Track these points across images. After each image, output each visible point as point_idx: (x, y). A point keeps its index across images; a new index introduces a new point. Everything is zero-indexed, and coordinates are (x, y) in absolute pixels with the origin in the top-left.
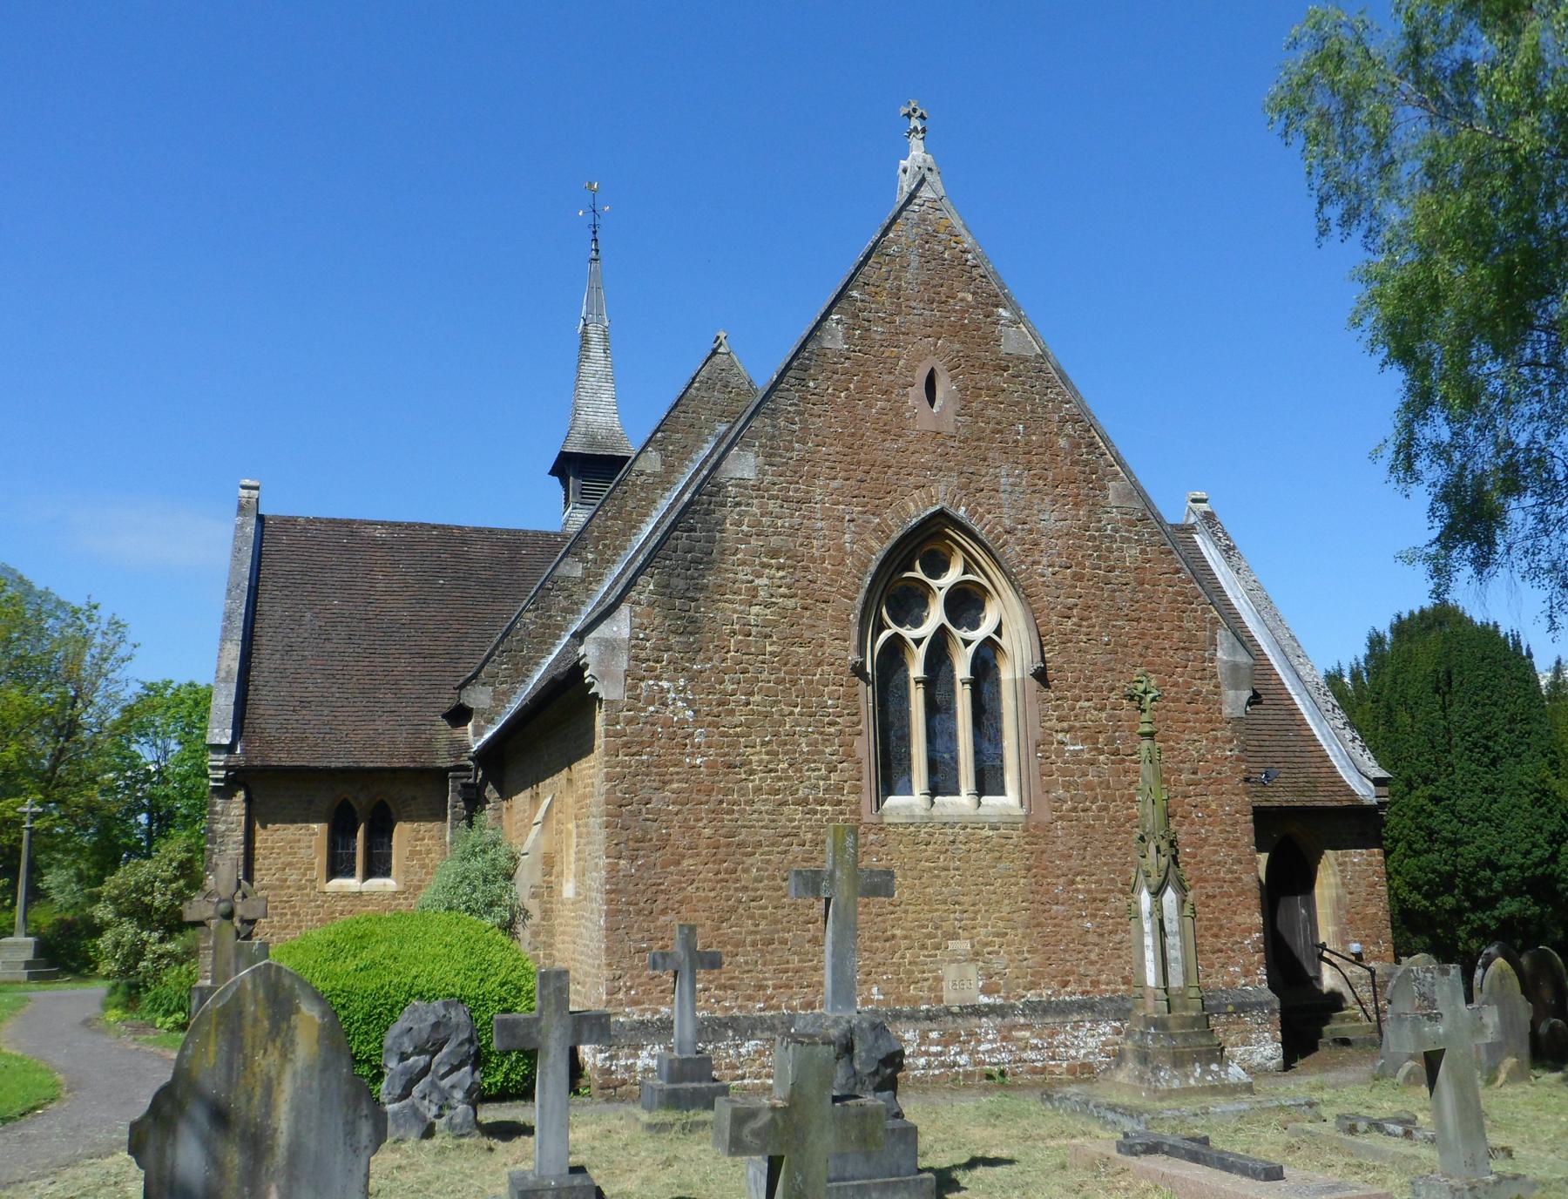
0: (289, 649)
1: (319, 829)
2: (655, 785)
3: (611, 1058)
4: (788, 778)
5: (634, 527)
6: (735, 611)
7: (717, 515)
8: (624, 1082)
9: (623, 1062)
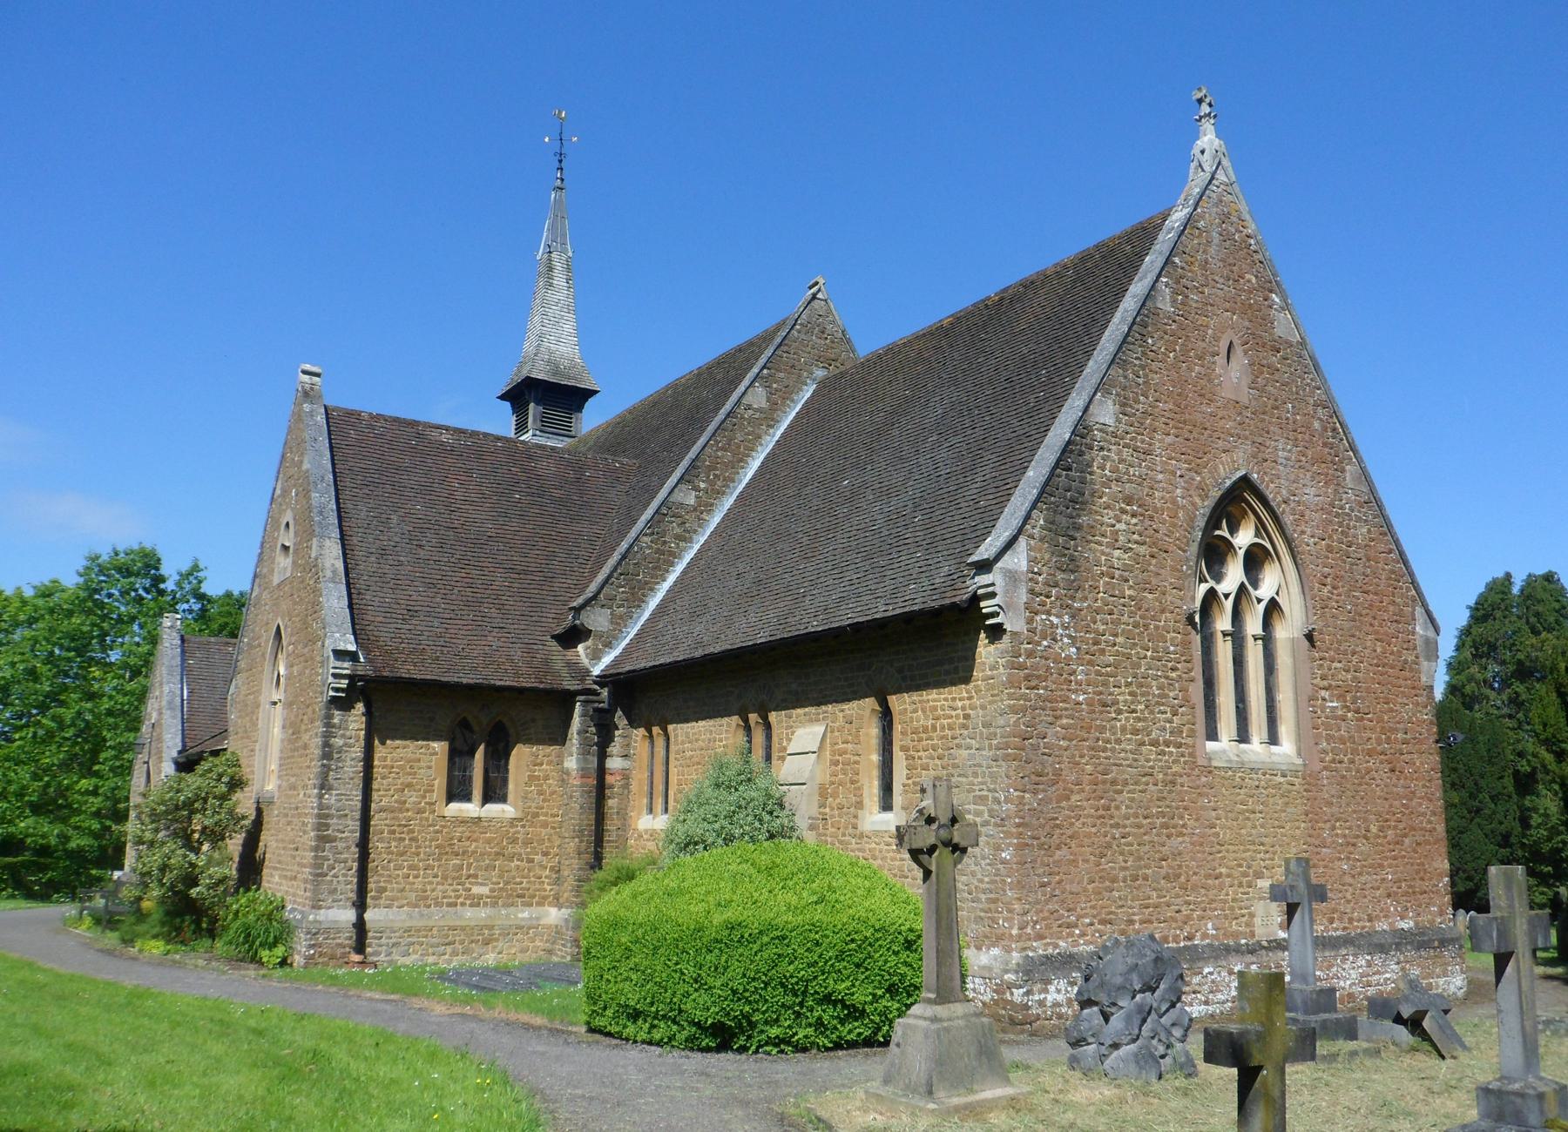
0: (383, 553)
1: (440, 747)
2: (1050, 719)
3: (1028, 993)
4: (1145, 720)
5: (740, 460)
6: (1103, 553)
7: (1087, 457)
8: (1038, 1017)
9: (1036, 997)
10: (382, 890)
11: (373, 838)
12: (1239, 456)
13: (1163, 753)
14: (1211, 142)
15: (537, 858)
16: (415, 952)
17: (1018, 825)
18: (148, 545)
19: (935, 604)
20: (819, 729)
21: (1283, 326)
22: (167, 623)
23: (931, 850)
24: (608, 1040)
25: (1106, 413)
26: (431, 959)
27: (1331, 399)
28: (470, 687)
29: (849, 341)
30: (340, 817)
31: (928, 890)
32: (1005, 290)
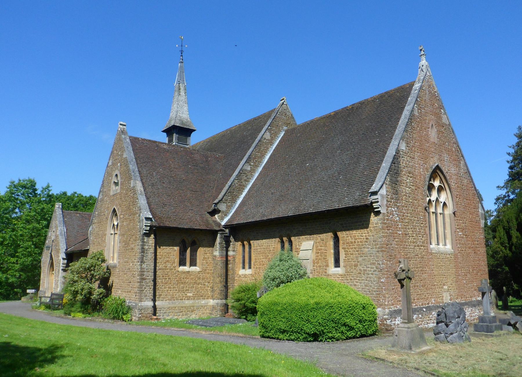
1: (177, 249)
3: (391, 321)
5: (263, 156)
10: (160, 295)
11: (158, 278)
12: (435, 159)
13: (420, 249)
14: (425, 63)
15: (206, 284)
16: (171, 315)
17: (387, 271)
18: (32, 178)
19: (358, 205)
20: (312, 243)
21: (444, 120)
22: (57, 206)
23: (403, 280)
24: (274, 340)
25: (403, 147)
26: (176, 317)
27: (457, 141)
28: (187, 229)
29: (293, 118)
30: (147, 272)
31: (403, 291)
32: (353, 105)
